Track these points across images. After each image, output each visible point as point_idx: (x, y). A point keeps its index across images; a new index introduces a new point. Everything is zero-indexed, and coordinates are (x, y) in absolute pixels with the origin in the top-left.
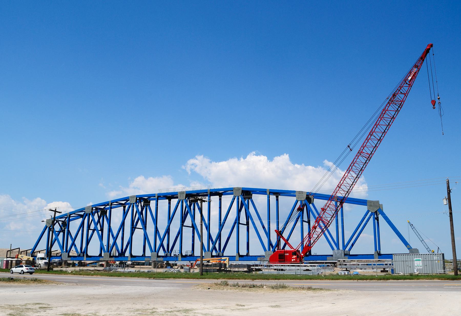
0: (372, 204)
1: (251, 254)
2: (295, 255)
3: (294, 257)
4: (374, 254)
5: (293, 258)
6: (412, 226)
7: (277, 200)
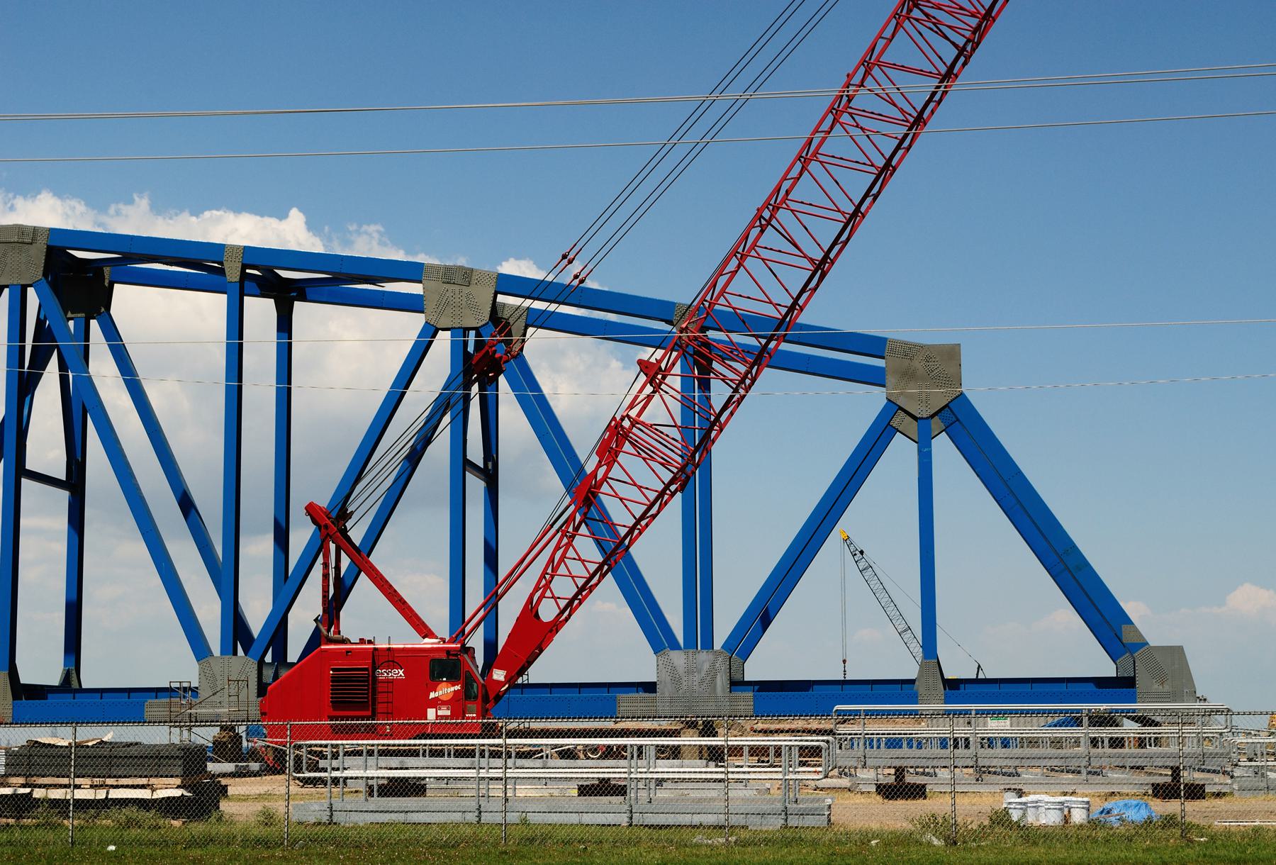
0: (918, 364)
1: (89, 680)
2: (453, 679)
3: (446, 690)
4: (912, 682)
5: (436, 699)
6: (859, 554)
7: (285, 325)
